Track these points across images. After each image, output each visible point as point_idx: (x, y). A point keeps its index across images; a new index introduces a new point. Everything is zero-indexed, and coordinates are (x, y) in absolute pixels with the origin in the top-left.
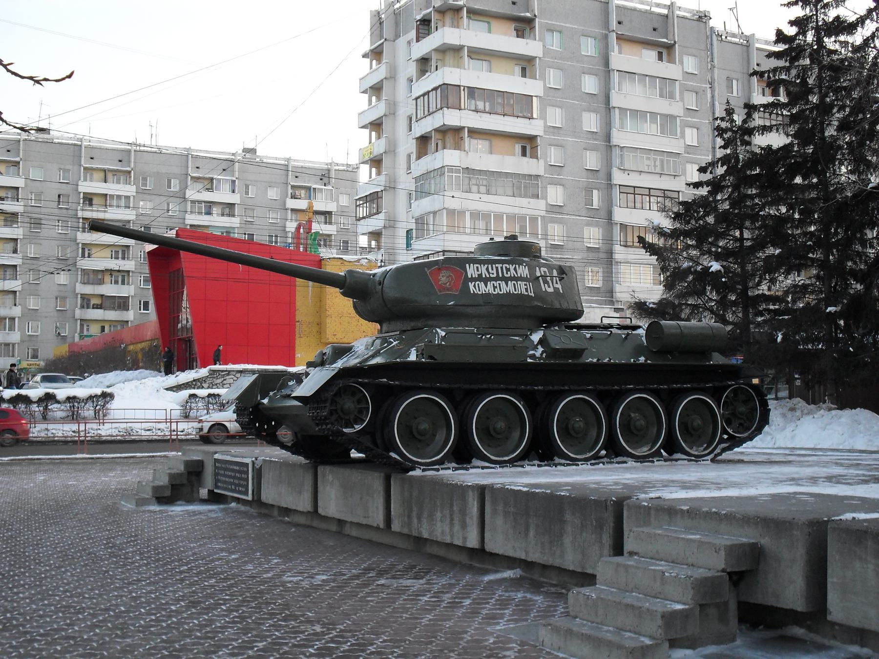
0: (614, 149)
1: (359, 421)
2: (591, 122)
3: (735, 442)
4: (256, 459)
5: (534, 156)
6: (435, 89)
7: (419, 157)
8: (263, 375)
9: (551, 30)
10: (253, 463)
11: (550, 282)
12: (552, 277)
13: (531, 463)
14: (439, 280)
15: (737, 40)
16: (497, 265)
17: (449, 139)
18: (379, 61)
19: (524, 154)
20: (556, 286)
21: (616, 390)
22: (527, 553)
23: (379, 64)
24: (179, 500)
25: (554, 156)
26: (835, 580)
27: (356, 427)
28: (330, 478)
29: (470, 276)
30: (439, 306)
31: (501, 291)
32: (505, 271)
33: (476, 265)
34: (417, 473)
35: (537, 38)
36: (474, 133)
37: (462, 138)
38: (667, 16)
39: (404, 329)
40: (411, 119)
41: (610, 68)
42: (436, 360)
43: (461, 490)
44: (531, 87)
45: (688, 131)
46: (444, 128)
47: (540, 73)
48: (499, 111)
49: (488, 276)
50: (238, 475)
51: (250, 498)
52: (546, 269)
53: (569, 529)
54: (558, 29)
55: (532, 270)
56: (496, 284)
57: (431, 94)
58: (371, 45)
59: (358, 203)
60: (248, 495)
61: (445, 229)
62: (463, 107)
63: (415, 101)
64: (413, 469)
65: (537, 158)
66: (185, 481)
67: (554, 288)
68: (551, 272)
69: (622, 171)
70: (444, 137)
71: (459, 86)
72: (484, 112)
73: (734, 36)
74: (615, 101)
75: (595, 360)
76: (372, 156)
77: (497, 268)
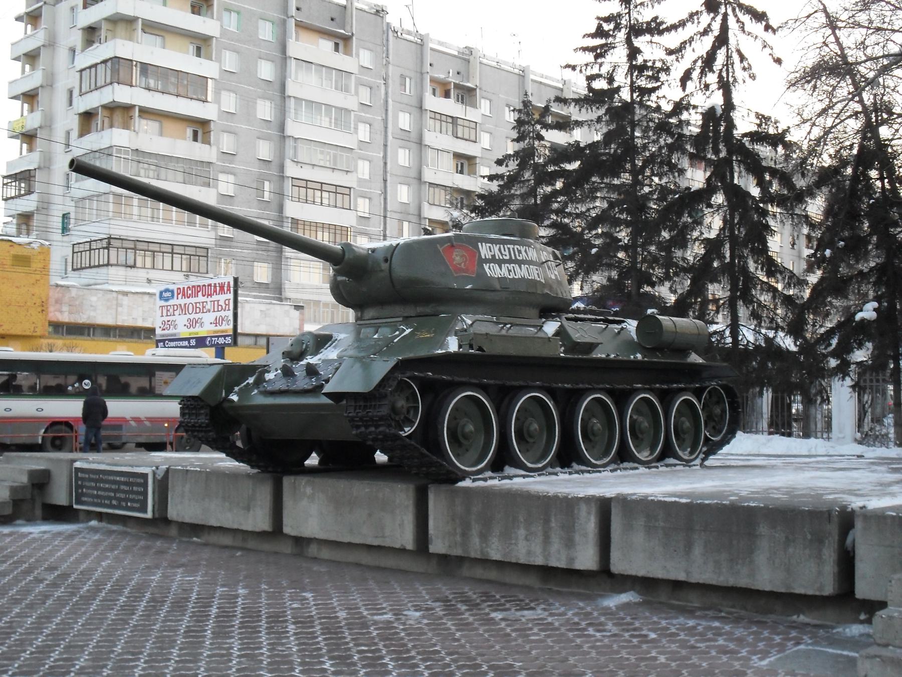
0: (287, 140)
1: (411, 423)
2: (265, 110)
3: (713, 448)
4: (157, 468)
5: (207, 141)
6: (105, 62)
7: (82, 135)
9: (229, 10)
10: (154, 473)
13: (564, 471)
14: (454, 260)
16: (509, 246)
18: (35, 26)
19: (195, 139)
21: (568, 390)
22: (688, 573)
23: (35, 29)
24: (18, 518)
25: (226, 143)
27: (406, 429)
28: (309, 490)
29: (483, 257)
30: (456, 289)
32: (517, 253)
33: (488, 245)
34: (467, 483)
35: (215, 17)
36: (145, 112)
37: (131, 117)
38: (345, 7)
41: (287, 55)
42: (484, 351)
43: (569, 504)
45: (361, 126)
46: (111, 106)
47: (216, 54)
48: (172, 91)
51: (149, 515)
53: (764, 544)
54: (236, 9)
56: (511, 266)
57: (99, 67)
58: (27, 8)
59: (6, 181)
60: (145, 512)
61: (111, 214)
62: (134, 84)
63: (78, 75)
64: (463, 479)
65: (209, 143)
69: (295, 164)
70: (112, 114)
71: (131, 61)
73: (409, 33)
74: (291, 90)
75: (604, 356)
76: (24, 130)
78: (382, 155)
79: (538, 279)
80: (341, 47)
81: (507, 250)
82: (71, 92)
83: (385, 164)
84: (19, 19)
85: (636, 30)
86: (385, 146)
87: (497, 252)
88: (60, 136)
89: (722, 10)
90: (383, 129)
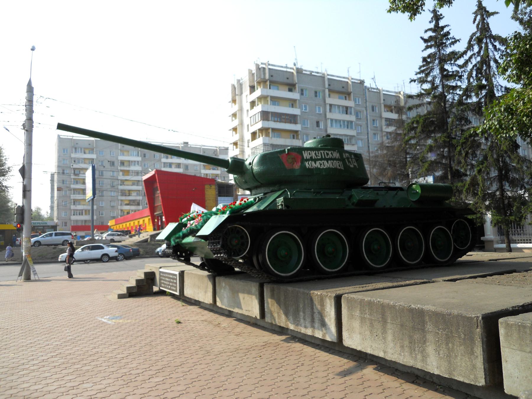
5: (297, 138)
15: (375, 90)
20: (354, 164)
29: (305, 158)
32: (326, 156)
33: (308, 152)
37: (269, 133)
39: (266, 192)
44: (296, 111)
49: (316, 158)
50: (172, 280)
53: (430, 337)
56: (321, 162)
66: (145, 284)
67: (354, 165)
68: (351, 156)
73: (374, 89)
74: (328, 117)
77: (321, 153)
78: (366, 137)
79: (339, 168)
80: (347, 98)
81: (320, 153)
82: (248, 125)
83: (368, 140)
84: (230, 102)
85: (443, 60)
86: (368, 133)
88: (246, 141)
89: (484, 41)
90: (366, 127)
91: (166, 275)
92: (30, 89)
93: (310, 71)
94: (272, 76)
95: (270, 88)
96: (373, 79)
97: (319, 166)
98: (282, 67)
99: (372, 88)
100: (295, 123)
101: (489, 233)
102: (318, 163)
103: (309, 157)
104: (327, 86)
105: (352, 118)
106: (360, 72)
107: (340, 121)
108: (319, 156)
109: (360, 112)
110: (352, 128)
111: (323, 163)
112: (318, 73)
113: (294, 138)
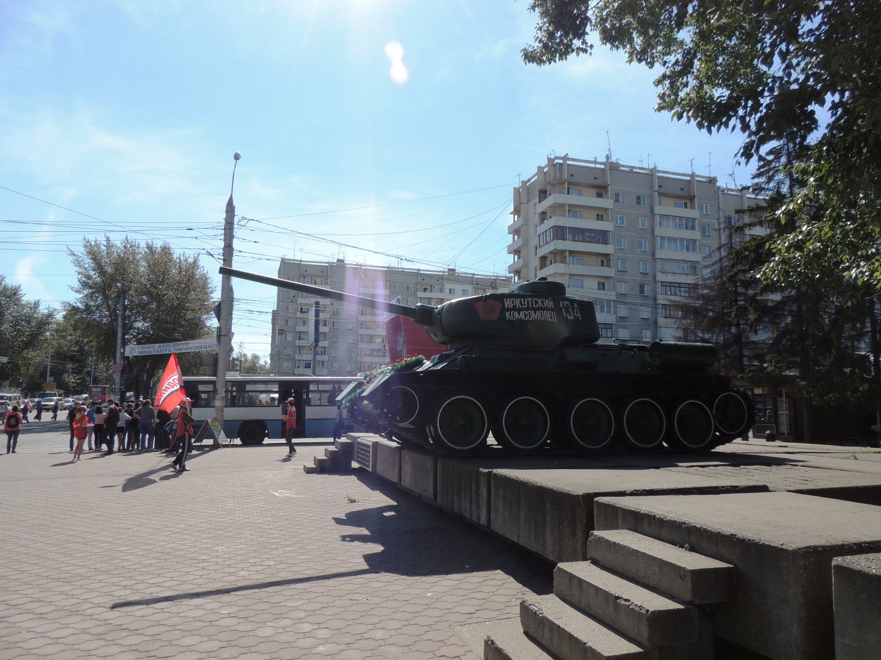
0: (657, 261)
5: (609, 266)
7: (541, 269)
8: (356, 376)
11: (572, 312)
12: (573, 310)
15: (735, 193)
17: (558, 258)
19: (602, 265)
20: (576, 315)
26: (846, 641)
29: (506, 307)
31: (530, 318)
37: (565, 257)
38: (689, 181)
40: (537, 247)
46: (554, 251)
49: (521, 307)
52: (568, 303)
55: (556, 304)
68: (572, 305)
70: (555, 256)
72: (579, 241)
73: (732, 190)
74: (656, 234)
77: (528, 301)
80: (689, 204)
87: (518, 302)
91: (362, 447)
92: (230, 208)
93: (630, 167)
94: (572, 175)
95: (568, 193)
96: (731, 175)
97: (523, 318)
98: (587, 162)
99: (729, 189)
100: (605, 242)
101: (785, 416)
102: (522, 313)
103: (511, 306)
104: (656, 188)
105: (696, 235)
106: (710, 166)
107: (675, 239)
108: (525, 305)
109: (709, 226)
110: (694, 250)
111: (529, 313)
112: (642, 169)
113: (602, 265)
